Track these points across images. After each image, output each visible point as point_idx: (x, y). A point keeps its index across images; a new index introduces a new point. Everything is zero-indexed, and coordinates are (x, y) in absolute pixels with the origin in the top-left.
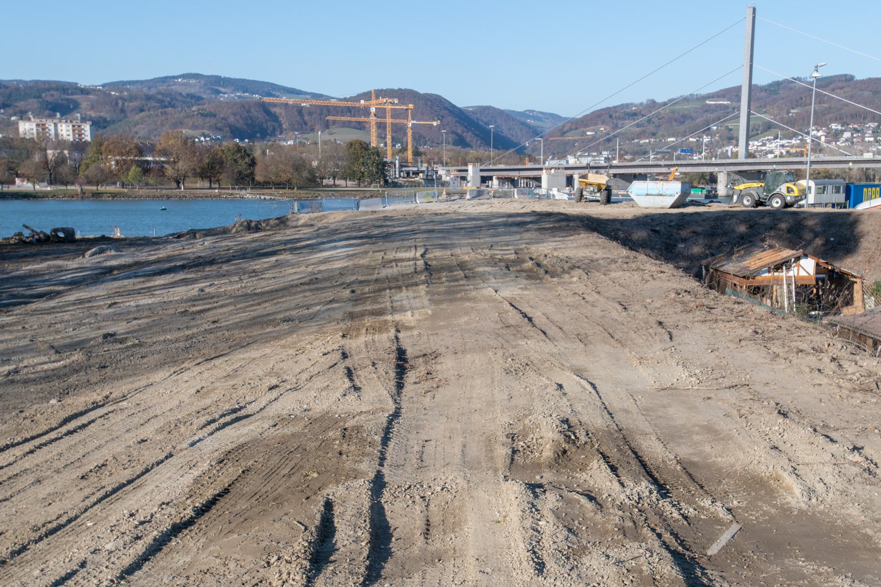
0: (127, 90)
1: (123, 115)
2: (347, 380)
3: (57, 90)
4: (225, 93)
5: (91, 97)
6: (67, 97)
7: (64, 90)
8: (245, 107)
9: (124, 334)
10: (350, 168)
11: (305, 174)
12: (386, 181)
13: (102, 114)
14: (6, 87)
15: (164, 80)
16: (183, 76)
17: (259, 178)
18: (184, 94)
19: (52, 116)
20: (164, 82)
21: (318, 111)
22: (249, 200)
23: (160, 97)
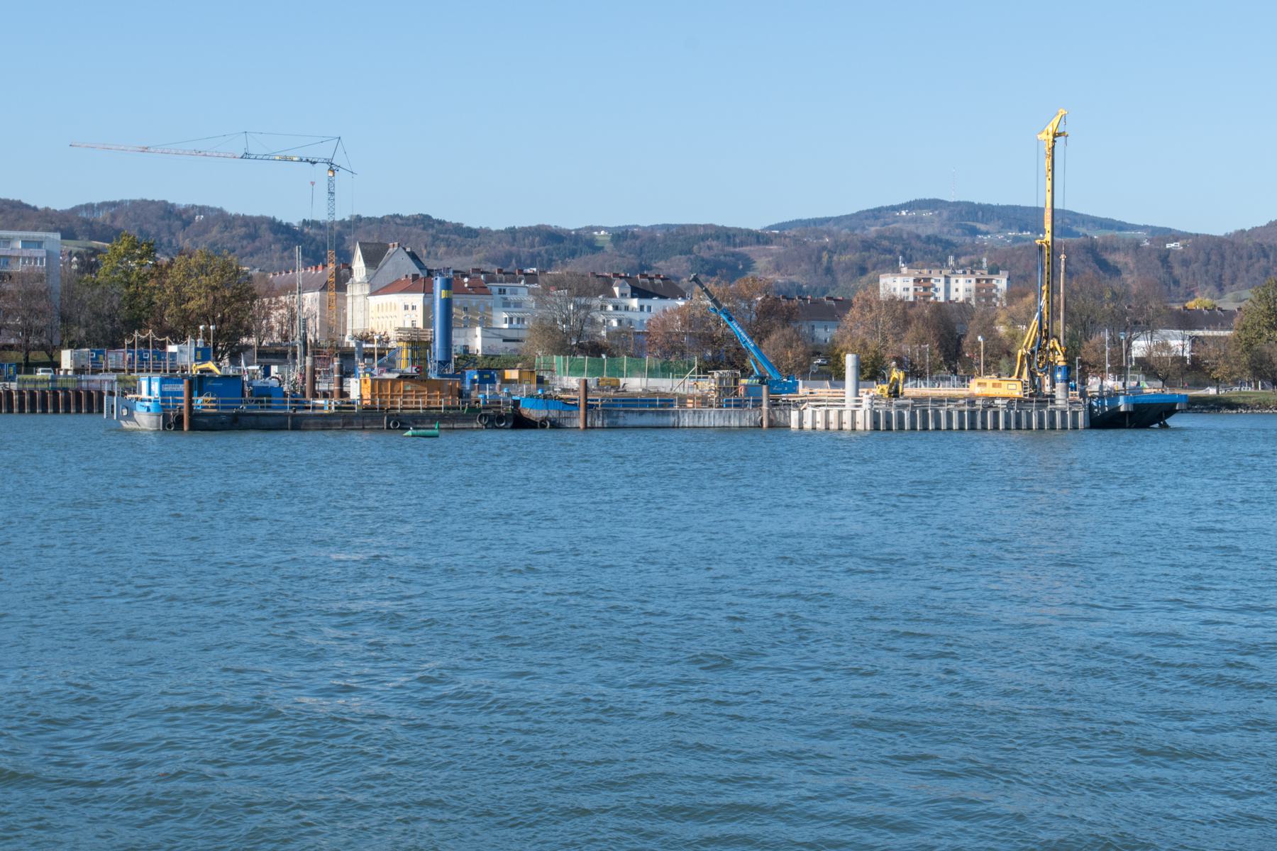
0: (829, 234)
1: (829, 278)
3: (718, 237)
4: (986, 233)
5: (774, 247)
6: (732, 249)
7: (729, 237)
13: (794, 278)
14: (635, 237)
15: (876, 214)
16: (909, 206)
18: (923, 236)
19: (942, 263)
20: (877, 218)
21: (1202, 256)
23: (886, 243)
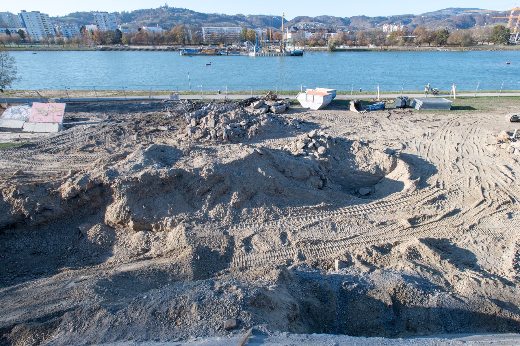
2: (496, 298)
8: (464, 17)
9: (140, 94)
10: (492, 37)
11: (468, 40)
12: (508, 43)
15: (440, 11)
17: (448, 42)
22: (441, 52)
